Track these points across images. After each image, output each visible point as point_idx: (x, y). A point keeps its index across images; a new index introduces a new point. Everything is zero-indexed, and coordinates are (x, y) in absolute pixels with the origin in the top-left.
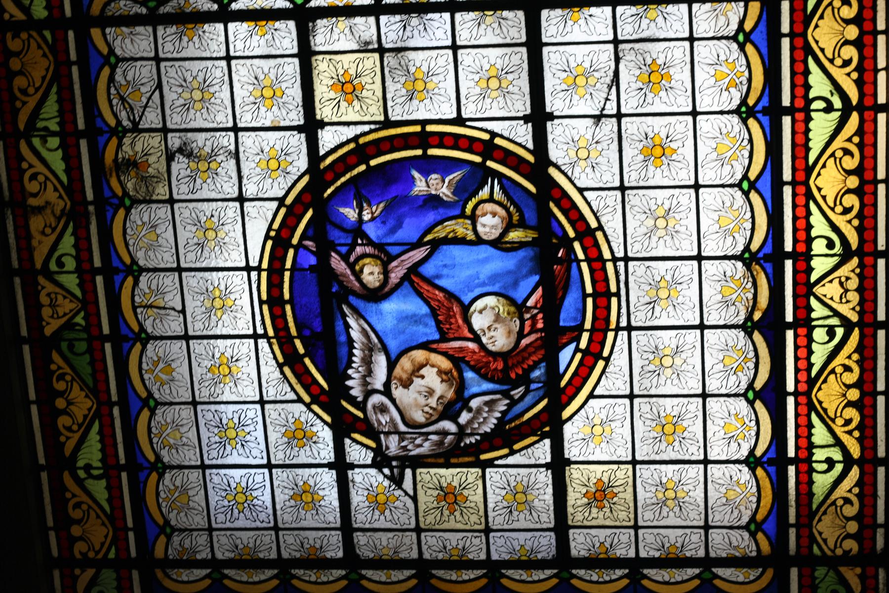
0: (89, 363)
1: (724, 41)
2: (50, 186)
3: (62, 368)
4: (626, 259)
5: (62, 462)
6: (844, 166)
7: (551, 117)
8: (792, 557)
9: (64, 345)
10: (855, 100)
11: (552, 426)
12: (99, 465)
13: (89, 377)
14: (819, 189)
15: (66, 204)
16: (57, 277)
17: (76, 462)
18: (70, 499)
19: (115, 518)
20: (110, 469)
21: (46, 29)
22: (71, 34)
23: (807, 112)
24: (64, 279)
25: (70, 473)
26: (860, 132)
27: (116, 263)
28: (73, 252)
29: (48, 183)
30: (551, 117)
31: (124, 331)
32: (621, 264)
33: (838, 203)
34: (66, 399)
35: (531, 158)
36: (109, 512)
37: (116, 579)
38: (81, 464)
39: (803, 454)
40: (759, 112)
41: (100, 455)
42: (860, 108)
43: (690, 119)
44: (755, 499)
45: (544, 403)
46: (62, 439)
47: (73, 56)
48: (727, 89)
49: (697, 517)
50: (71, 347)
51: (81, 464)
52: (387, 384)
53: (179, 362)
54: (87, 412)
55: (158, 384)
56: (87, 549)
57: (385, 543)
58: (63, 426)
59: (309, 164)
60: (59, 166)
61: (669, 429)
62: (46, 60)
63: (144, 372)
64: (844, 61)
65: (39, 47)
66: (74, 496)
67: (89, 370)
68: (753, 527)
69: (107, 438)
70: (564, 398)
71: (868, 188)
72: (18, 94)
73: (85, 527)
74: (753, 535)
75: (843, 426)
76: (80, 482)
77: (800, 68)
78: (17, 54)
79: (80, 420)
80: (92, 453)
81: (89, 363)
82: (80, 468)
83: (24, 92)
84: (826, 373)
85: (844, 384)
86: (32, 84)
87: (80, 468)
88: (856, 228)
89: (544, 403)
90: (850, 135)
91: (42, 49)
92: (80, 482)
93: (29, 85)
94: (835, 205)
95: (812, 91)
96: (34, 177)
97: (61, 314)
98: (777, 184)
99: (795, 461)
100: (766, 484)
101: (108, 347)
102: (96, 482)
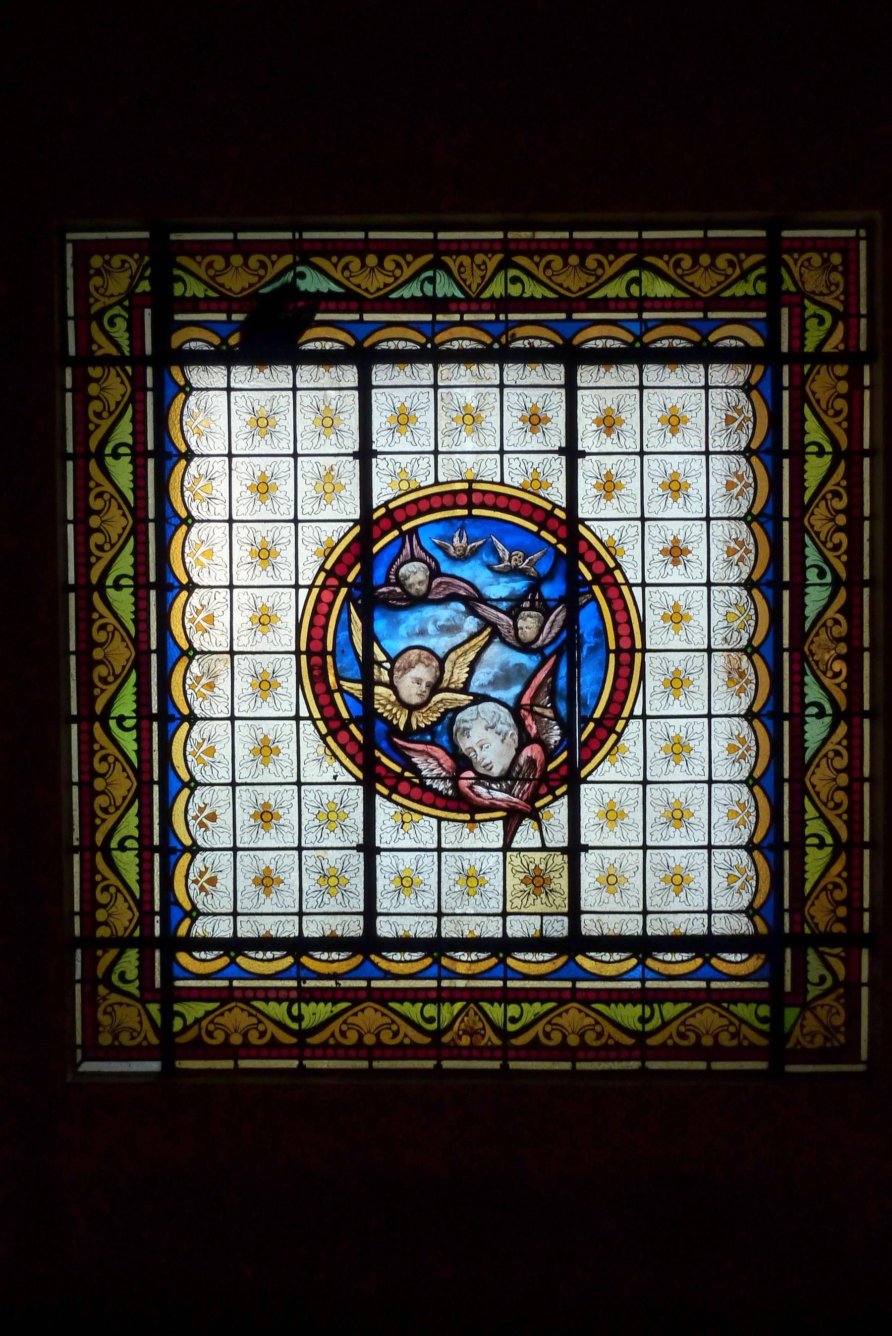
1: (205, 584)
4: (297, 718)
5: (847, 457)
6: (107, 798)
7: (355, 455)
8: (157, 938)
10: (97, 725)
11: (369, 524)
14: (128, 777)
19: (800, 398)
20: (798, 454)
21: (807, 935)
22: (786, 234)
26: (90, 566)
27: (769, 592)
30: (355, 455)
31: (770, 723)
32: (304, 712)
34: (835, 915)
35: (379, 787)
36: (806, 406)
37: (805, 480)
39: (142, 593)
40: (178, 719)
42: (94, 849)
43: (239, 845)
44: (185, 429)
47: (786, 656)
48: (206, 805)
53: (718, 429)
55: (739, 407)
57: (535, 373)
59: (578, 616)
60: (811, 424)
61: (262, 422)
63: (753, 485)
64: (102, 497)
65: (818, 401)
68: (188, 389)
70: (356, 549)
71: (86, 778)
74: (188, 383)
75: (107, 624)
76: (834, 442)
77: (142, 627)
80: (815, 468)
84: (117, 413)
85: (109, 926)
88: (96, 742)
89: (376, 549)
91: (815, 532)
92: (834, 442)
95: (135, 736)
98: (162, 651)
99: (153, 718)
100: (175, 433)
101: (786, 709)
102: (817, 700)
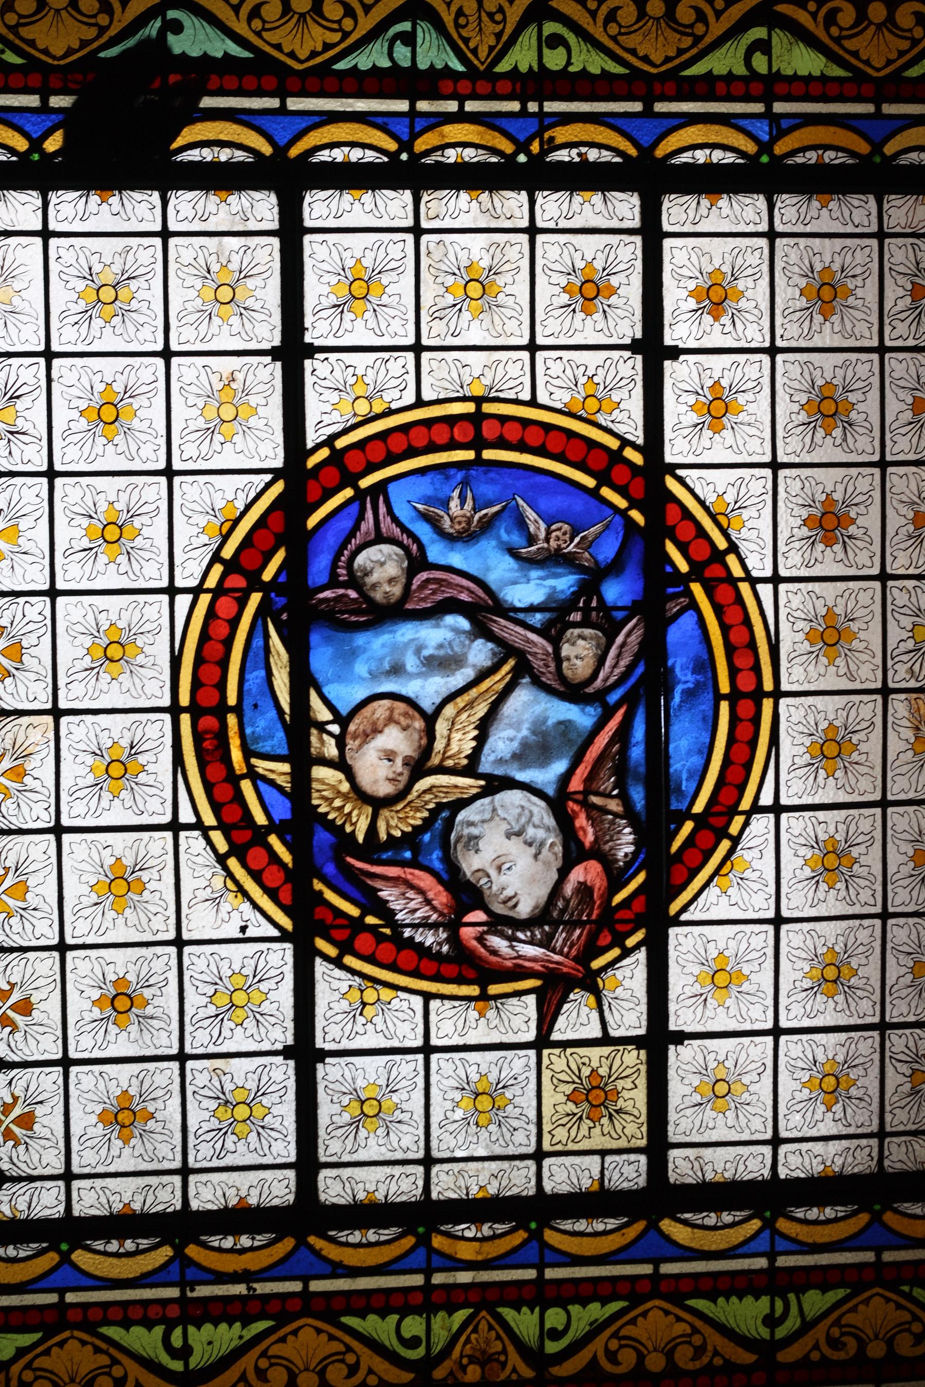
0: (584, 1306)
2: (849, 1319)
3: (244, 1372)
9: (552, 1347)
12: (765, 1300)
13: (607, 1307)
15: (878, 1294)
16: (436, 1349)
17: (763, 1340)
18: (822, 1354)
23: (775, 77)
24: (440, 1337)
25: (554, 1365)
28: (394, 1318)
29: (36, 1364)
33: (92, 21)
38: (765, 1333)
41: (749, 1299)
45: (313, 521)
46: (372, 1380)
49: (62, 252)
50: (555, 1335)
51: (765, 1333)
52: (586, 792)
54: (892, 1305)
56: (907, 1334)
58: (692, 1359)
62: (651, 1313)
66: (816, 1347)
67: (595, 1307)
69: (128, 1315)
72: (705, 1360)
73: (651, 1348)
78: (641, 1357)
79: (105, 1360)
81: (584, 1306)
82: (772, 1334)
83: (699, 1351)
86: (341, 1357)
87: (772, 1334)
90: (229, 8)
91: (856, 1306)
93: (689, 1343)
94: (96, 25)
96: (612, 1357)
97: (498, 1347)
